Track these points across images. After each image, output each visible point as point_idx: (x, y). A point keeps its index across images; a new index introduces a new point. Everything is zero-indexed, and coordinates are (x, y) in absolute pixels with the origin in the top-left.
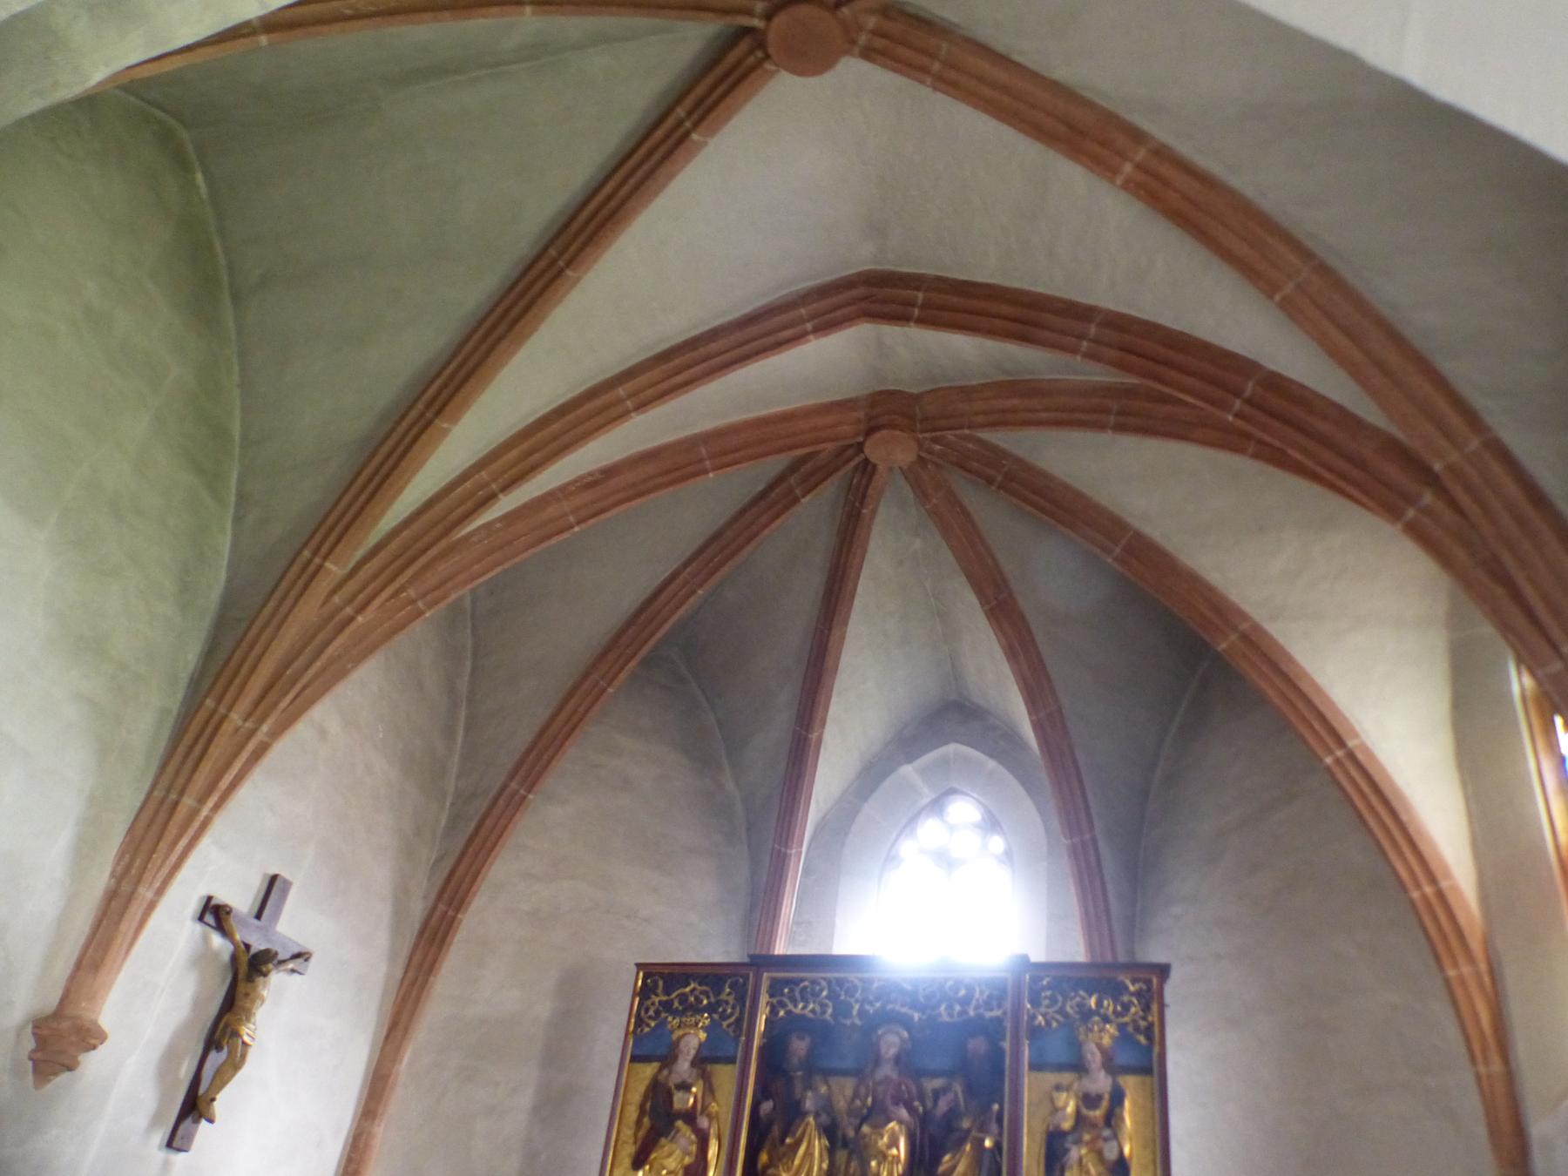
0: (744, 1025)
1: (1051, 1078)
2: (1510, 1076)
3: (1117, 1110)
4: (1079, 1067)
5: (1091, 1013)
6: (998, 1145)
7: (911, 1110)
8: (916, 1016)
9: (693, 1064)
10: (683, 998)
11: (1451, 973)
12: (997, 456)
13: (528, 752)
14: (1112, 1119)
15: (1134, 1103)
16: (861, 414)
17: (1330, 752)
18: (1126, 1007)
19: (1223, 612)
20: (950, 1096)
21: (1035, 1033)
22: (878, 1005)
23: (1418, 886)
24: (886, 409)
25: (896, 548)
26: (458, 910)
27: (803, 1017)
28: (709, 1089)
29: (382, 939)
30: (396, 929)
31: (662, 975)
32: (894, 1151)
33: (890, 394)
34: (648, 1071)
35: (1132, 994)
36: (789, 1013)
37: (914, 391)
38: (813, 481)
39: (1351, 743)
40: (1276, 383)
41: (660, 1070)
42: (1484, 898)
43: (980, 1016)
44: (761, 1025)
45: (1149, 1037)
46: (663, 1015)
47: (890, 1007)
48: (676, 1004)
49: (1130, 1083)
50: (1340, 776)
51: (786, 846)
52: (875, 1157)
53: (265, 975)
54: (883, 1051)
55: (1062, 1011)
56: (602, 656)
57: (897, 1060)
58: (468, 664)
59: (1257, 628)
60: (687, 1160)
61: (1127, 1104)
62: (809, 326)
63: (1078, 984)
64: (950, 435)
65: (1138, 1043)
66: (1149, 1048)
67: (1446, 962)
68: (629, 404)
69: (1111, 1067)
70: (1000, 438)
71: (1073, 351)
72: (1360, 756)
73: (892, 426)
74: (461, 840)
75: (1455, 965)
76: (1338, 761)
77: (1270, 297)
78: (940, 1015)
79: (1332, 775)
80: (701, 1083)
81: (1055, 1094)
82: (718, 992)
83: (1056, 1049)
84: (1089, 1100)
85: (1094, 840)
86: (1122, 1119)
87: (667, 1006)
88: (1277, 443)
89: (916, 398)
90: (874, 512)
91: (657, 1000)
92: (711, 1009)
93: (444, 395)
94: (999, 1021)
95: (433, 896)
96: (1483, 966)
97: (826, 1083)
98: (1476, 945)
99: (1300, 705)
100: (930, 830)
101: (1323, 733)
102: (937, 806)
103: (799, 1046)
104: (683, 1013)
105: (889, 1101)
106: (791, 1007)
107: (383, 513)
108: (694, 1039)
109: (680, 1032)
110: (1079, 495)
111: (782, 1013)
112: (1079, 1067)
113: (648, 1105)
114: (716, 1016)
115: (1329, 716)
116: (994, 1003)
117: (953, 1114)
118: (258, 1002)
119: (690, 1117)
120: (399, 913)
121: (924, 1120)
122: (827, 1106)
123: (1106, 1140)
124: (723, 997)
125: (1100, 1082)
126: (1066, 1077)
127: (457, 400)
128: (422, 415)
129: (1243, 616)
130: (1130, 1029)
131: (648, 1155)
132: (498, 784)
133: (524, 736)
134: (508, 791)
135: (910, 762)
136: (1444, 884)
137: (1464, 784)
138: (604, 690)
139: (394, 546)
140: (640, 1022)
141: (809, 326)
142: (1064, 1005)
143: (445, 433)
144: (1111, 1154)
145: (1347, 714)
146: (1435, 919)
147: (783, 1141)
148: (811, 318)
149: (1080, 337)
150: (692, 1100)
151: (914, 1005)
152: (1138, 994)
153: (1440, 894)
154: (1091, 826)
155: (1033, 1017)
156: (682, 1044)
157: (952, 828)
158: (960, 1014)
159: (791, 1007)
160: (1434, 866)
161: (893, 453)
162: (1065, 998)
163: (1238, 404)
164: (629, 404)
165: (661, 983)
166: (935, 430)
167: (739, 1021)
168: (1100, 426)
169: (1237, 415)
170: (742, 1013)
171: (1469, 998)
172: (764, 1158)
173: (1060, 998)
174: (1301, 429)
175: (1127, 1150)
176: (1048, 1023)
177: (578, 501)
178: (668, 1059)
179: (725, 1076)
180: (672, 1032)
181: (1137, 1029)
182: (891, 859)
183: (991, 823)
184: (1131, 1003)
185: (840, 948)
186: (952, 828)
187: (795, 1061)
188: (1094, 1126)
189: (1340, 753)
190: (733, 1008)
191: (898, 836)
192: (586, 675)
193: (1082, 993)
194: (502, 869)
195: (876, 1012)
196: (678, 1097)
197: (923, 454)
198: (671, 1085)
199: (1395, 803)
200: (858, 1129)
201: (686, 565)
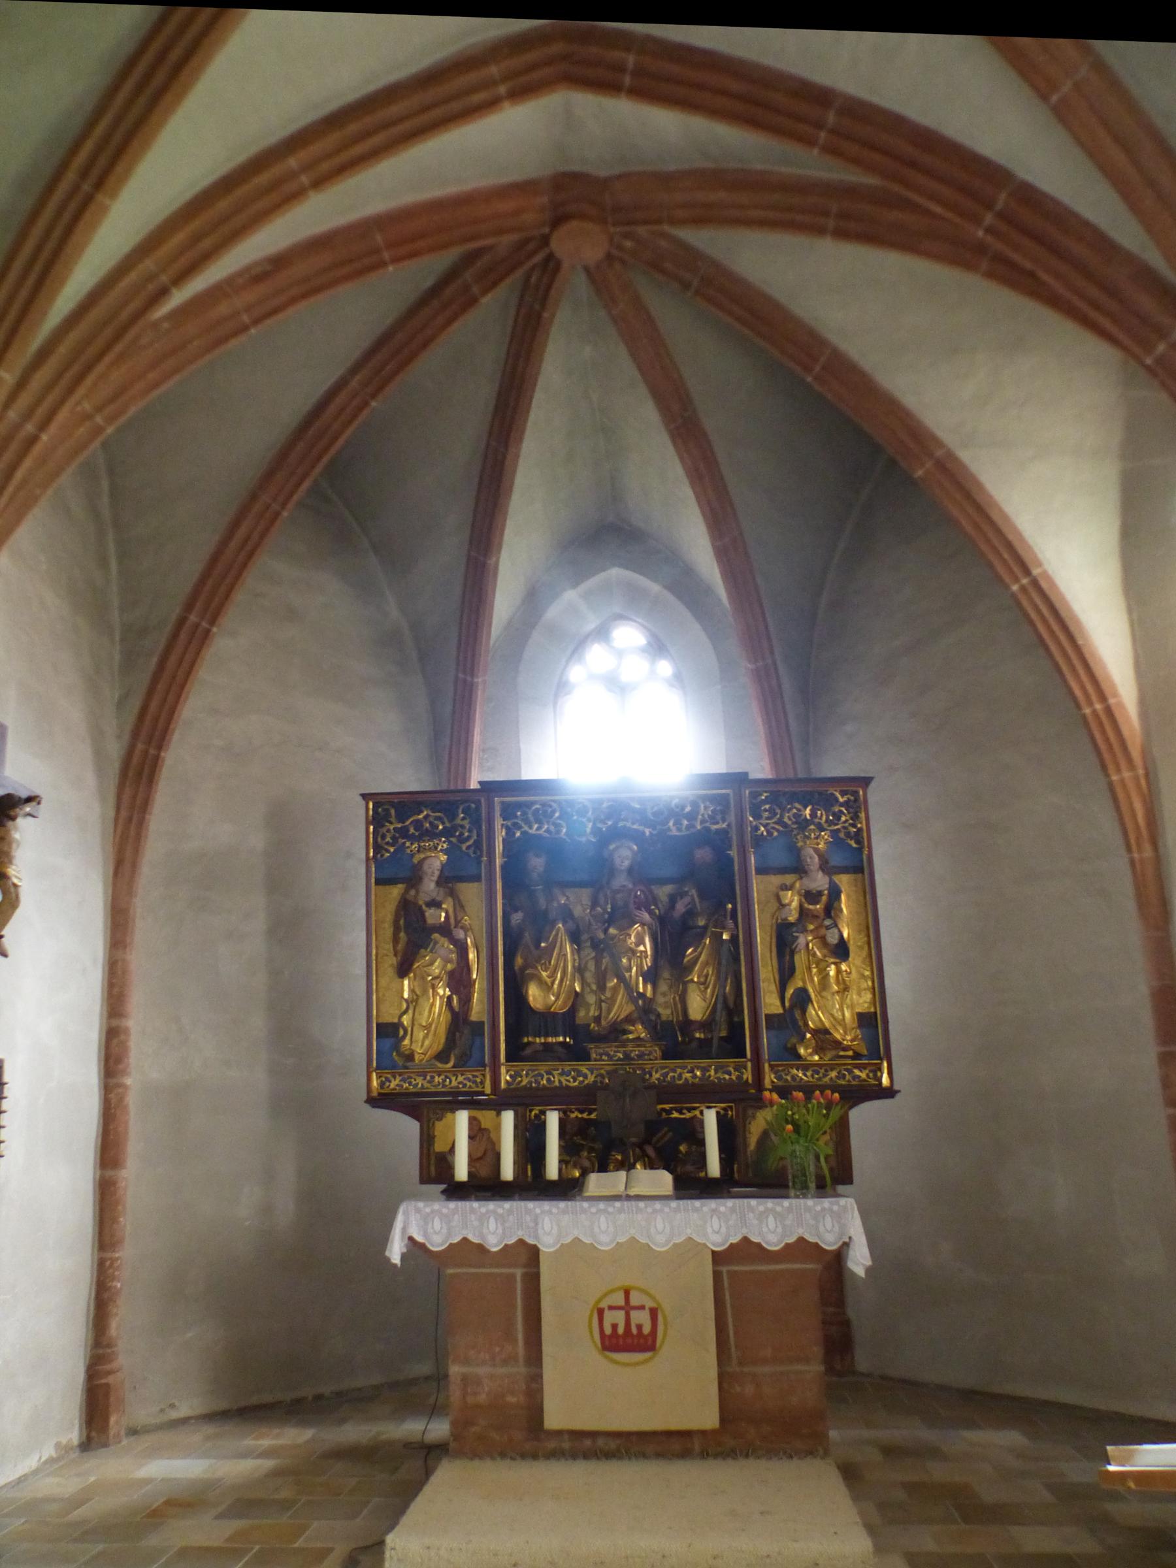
0: (482, 846)
1: (776, 880)
2: (1158, 860)
3: (836, 904)
4: (799, 870)
5: (807, 823)
6: (734, 939)
7: (651, 913)
8: (647, 832)
9: (438, 883)
10: (418, 825)
11: (1115, 778)
12: (692, 257)
13: (202, 581)
14: (831, 910)
15: (848, 897)
16: (545, 200)
17: (1017, 580)
18: (837, 816)
19: (919, 438)
20: (687, 900)
21: (758, 841)
22: (610, 823)
23: (1090, 704)
24: (570, 195)
25: (575, 362)
26: (160, 748)
27: (540, 837)
28: (459, 905)
29: (90, 779)
30: (100, 771)
31: (392, 804)
32: (642, 948)
33: (576, 177)
34: (396, 891)
35: (842, 805)
36: (524, 833)
37: (603, 173)
38: (491, 278)
39: (1036, 572)
40: (1028, 195)
41: (407, 891)
42: (1144, 714)
43: (708, 830)
44: (499, 847)
45: (857, 842)
46: (401, 841)
47: (621, 824)
48: (412, 831)
49: (844, 881)
50: (1025, 603)
51: (472, 675)
52: (625, 954)
53: (13, 819)
54: (617, 861)
55: (780, 822)
56: (269, 475)
57: (630, 871)
58: (105, 484)
59: (951, 455)
60: (449, 967)
61: (843, 897)
62: (502, 89)
63: (793, 797)
64: (642, 231)
65: (850, 846)
66: (860, 850)
67: (1111, 768)
68: (304, 179)
69: (826, 867)
70: (698, 238)
71: (810, 142)
72: (1044, 585)
73: (583, 217)
74: (145, 678)
75: (1119, 770)
76: (1023, 589)
77: (1044, 97)
78: (669, 829)
79: (1019, 604)
80: (450, 900)
81: (782, 893)
82: (453, 816)
83: (779, 856)
84: (811, 896)
85: (775, 663)
86: (841, 910)
87: (403, 833)
88: (1028, 265)
89: (604, 184)
90: (553, 315)
91: (392, 827)
92: (448, 833)
93: (103, 161)
94: (725, 832)
95: (127, 737)
96: (1141, 772)
97: (564, 895)
98: (1136, 754)
99: (991, 534)
100: (597, 656)
101: (1011, 562)
102: (602, 633)
103: (537, 863)
104: (419, 839)
105: (632, 906)
106: (526, 828)
107: (45, 313)
108: (437, 860)
109: (422, 856)
110: (776, 306)
111: (518, 834)
112: (799, 870)
113: (402, 922)
114: (453, 840)
115: (1016, 544)
116: (719, 817)
117: (691, 913)
118: (14, 846)
119: (445, 930)
120: (99, 753)
121: (662, 920)
122: (567, 914)
123: (828, 928)
124: (458, 821)
125: (820, 881)
126: (789, 879)
127: (119, 168)
128: (76, 188)
129: (939, 443)
130: (842, 835)
131: (411, 965)
132: (174, 617)
133: (191, 568)
134: (188, 624)
135: (575, 585)
136: (1112, 701)
137: (1130, 611)
138: (277, 514)
139: (63, 349)
140: (378, 848)
141: (502, 89)
142: (782, 816)
143: (104, 210)
144: (833, 939)
145: (1031, 541)
146: (1103, 732)
147: (538, 946)
148: (505, 78)
149: (819, 125)
150: (443, 914)
151: (645, 822)
152: (846, 804)
153: (1109, 711)
154: (772, 653)
155: (757, 829)
156: (425, 867)
157: (620, 654)
158: (688, 827)
159: (526, 828)
160: (1104, 686)
161: (580, 246)
162: (783, 809)
163: (989, 219)
164: (304, 179)
165: (393, 811)
166: (629, 223)
167: (477, 845)
168: (819, 231)
169: (989, 230)
170: (479, 835)
171: (1129, 797)
172: (519, 961)
173: (778, 811)
174: (1054, 250)
175: (845, 935)
176: (770, 833)
177: (250, 296)
178: (413, 878)
179: (472, 893)
180: (412, 856)
181: (848, 835)
182: (562, 687)
183: (657, 648)
184: (841, 812)
185: (529, 773)
186: (620, 654)
187: (535, 875)
188: (816, 917)
189: (1025, 581)
190: (470, 831)
191: (568, 662)
192: (253, 497)
193: (797, 805)
194: (194, 707)
195: (609, 828)
196: (430, 913)
197: (615, 252)
198: (421, 902)
199: (1072, 628)
200: (606, 931)
201: (354, 370)
